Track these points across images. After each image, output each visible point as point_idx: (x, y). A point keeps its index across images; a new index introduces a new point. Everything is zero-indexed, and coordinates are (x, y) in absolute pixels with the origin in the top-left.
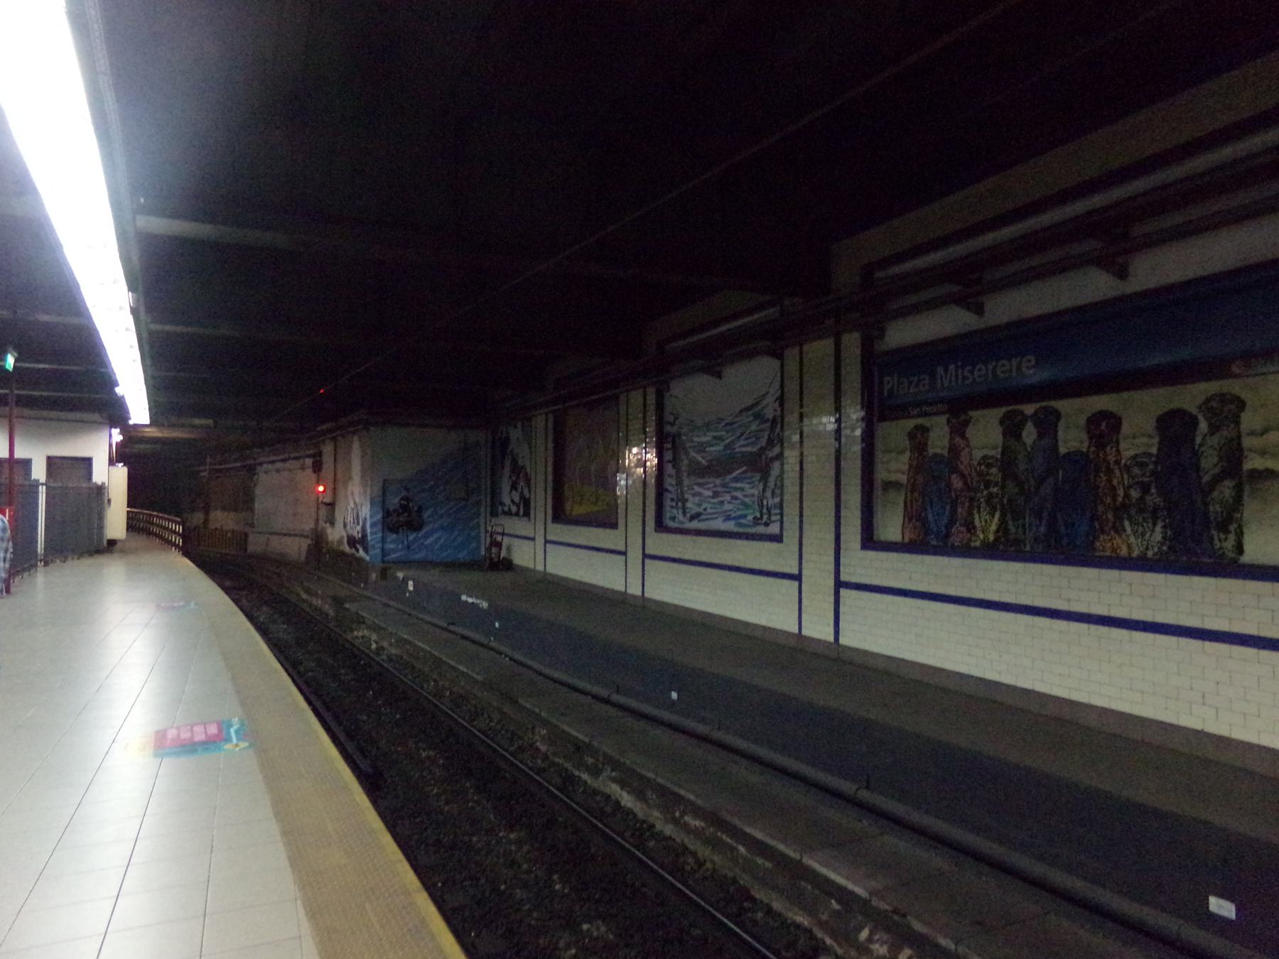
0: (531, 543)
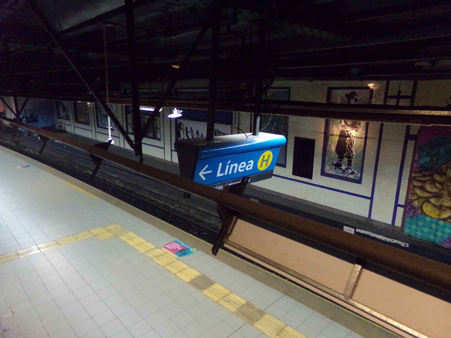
0: (91, 132)
